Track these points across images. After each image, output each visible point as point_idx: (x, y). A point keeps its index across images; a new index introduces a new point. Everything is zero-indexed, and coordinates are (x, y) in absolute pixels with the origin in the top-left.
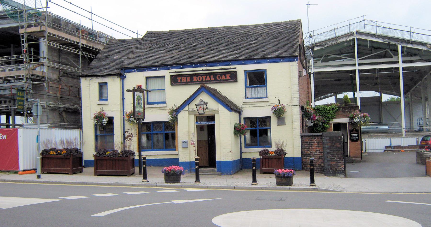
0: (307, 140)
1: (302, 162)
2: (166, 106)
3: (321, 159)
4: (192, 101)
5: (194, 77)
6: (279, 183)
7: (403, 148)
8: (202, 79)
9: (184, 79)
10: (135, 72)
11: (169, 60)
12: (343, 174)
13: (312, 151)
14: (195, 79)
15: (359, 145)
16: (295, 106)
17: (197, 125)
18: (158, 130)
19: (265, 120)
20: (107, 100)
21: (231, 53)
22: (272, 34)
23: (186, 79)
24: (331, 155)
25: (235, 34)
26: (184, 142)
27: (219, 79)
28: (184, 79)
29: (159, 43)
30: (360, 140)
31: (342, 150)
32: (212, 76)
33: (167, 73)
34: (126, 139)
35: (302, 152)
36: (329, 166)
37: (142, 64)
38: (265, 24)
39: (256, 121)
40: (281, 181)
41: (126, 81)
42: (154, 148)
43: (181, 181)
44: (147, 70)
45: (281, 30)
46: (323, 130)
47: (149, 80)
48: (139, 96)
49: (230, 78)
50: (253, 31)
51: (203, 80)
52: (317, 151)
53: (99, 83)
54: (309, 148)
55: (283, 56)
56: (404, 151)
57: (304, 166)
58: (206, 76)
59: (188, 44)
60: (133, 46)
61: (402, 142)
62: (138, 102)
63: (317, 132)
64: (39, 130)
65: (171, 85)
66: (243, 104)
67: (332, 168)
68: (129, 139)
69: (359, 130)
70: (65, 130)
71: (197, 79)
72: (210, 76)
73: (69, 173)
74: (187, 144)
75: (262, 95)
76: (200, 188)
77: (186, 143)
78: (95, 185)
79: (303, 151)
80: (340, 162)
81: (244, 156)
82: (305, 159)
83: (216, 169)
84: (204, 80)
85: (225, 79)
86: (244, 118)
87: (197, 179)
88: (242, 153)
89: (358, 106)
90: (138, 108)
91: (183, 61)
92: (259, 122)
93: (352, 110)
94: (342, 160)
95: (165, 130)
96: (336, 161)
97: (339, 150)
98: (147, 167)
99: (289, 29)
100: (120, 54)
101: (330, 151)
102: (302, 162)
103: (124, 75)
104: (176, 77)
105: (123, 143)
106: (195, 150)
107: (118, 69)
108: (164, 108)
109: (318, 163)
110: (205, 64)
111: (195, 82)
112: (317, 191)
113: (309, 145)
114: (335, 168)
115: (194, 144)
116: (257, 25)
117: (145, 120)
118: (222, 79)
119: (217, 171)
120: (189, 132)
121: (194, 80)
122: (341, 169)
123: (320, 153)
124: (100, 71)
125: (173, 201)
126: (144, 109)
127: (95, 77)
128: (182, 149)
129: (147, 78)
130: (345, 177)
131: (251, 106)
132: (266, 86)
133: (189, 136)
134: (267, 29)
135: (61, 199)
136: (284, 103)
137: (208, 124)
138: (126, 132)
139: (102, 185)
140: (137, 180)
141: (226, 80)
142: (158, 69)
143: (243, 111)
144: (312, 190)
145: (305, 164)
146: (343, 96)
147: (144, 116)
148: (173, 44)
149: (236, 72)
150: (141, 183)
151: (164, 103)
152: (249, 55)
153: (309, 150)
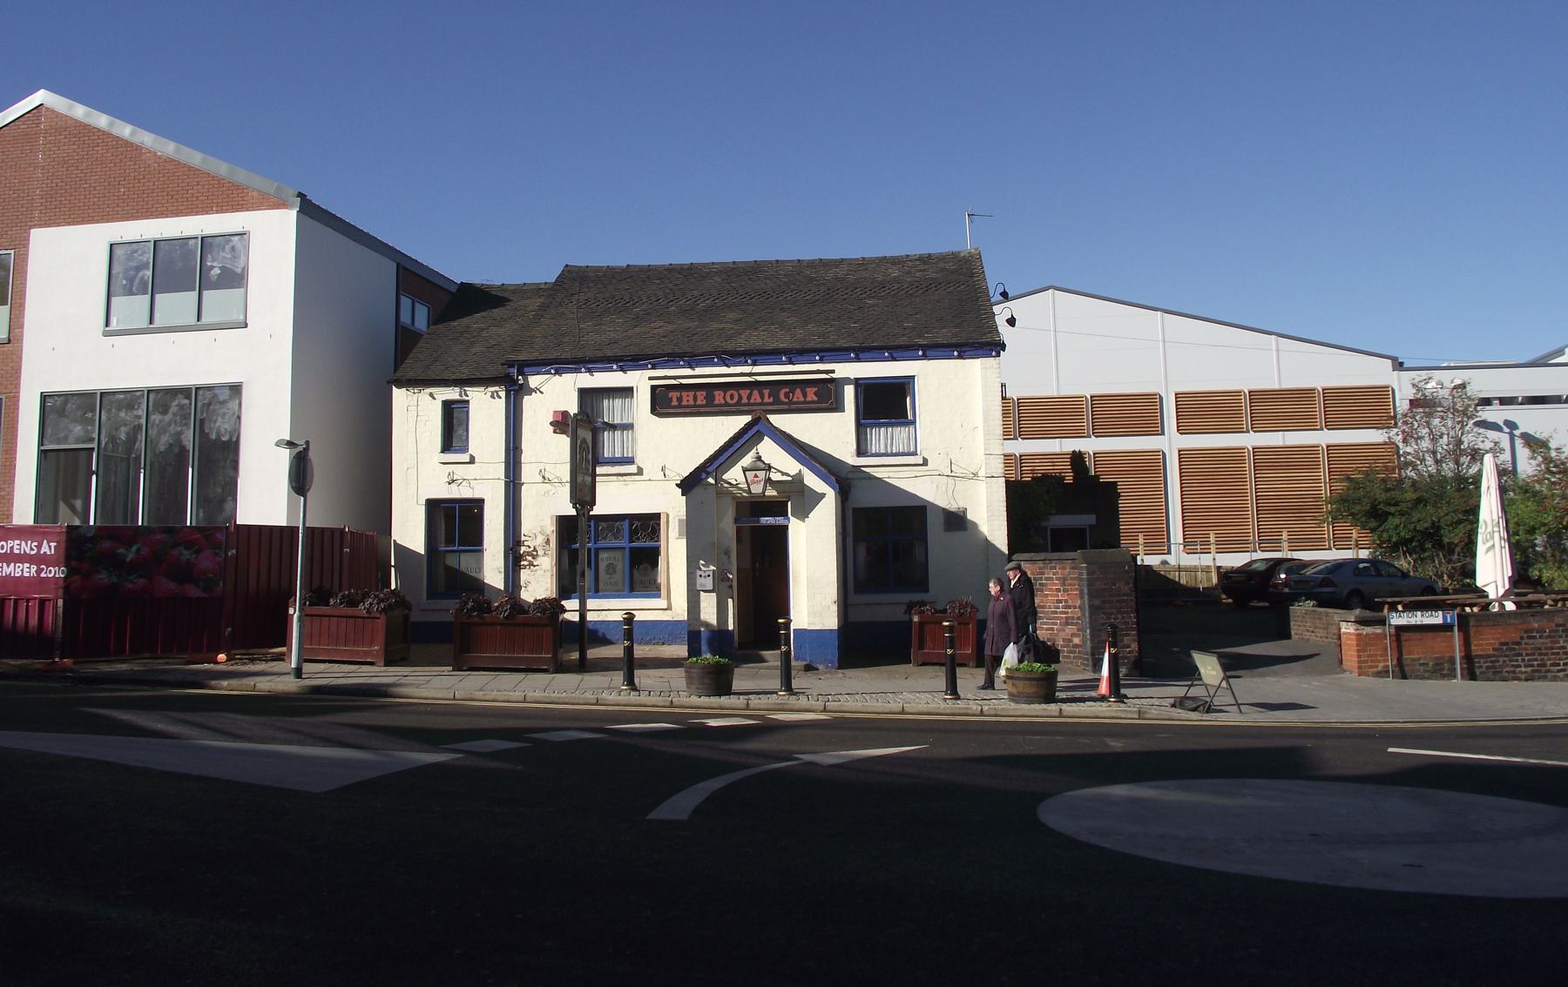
3: (1072, 624)
6: (1014, 696)
8: (740, 398)
14: (719, 397)
16: (993, 477)
24: (1104, 613)
27: (787, 400)
28: (688, 398)
32: (766, 392)
48: (584, 441)
49: (816, 399)
51: (743, 402)
52: (1060, 601)
71: (725, 400)
80: (1128, 635)
84: (745, 401)
89: (798, 479)
95: (631, 541)
117: (596, 511)
118: (795, 399)
121: (717, 402)
123: (1066, 607)
134: (895, 272)
141: (805, 402)
142: (817, 358)
151: (630, 461)
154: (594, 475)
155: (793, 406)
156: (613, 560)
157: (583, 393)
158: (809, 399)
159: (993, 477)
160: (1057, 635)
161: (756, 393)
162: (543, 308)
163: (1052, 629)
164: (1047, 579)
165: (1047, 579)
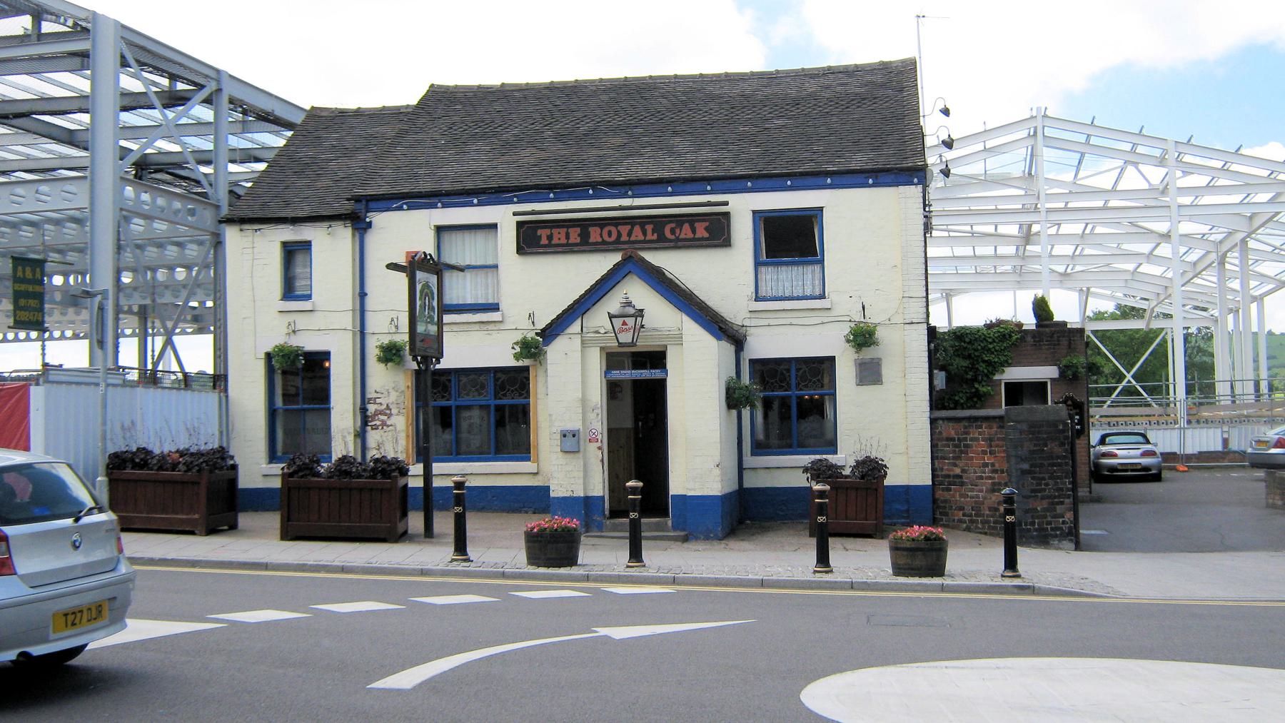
0: (953, 432)
1: (935, 501)
2: (501, 320)
4: (594, 305)
5: (591, 229)
7: (1182, 458)
8: (619, 235)
9: (559, 236)
10: (400, 208)
11: (510, 174)
12: (1071, 540)
13: (967, 465)
15: (1083, 450)
16: (912, 323)
17: (607, 381)
18: (474, 397)
19: (820, 369)
20: (309, 297)
21: (706, 154)
22: (831, 101)
23: (568, 237)
24: (1033, 478)
25: (712, 97)
26: (567, 434)
27: (673, 237)
28: (559, 236)
29: (473, 122)
30: (1086, 433)
31: (1067, 464)
32: (649, 228)
33: (505, 216)
34: (370, 424)
35: (933, 470)
36: (1028, 515)
37: (426, 186)
38: (803, 70)
39: (788, 371)
40: (909, 561)
41: (372, 238)
42: (458, 453)
43: (579, 562)
44: (439, 205)
45: (858, 90)
46: (974, 402)
47: (446, 237)
48: (426, 286)
49: (706, 235)
50: (768, 91)
51: (622, 239)
52: (986, 465)
53: (285, 245)
54: (959, 458)
55: (874, 167)
56: (1186, 469)
57: (941, 513)
58: (629, 227)
59: (567, 126)
60: (390, 131)
61: (1182, 442)
62: (425, 303)
63: (955, 408)
64: (106, 391)
65: (518, 252)
66: (748, 315)
67: (1036, 521)
68: (378, 423)
69: (1083, 403)
70: (152, 389)
71: (601, 237)
72: (644, 226)
73: (196, 532)
74: (579, 442)
75: (790, 288)
76: (653, 583)
77: (574, 436)
78: (295, 571)
79: (936, 466)
80: (1062, 503)
81: (752, 481)
82: (943, 490)
83: (670, 523)
84: (624, 238)
85: (690, 235)
86: (750, 360)
87: (636, 555)
88: (744, 472)
90: (423, 321)
91: (558, 179)
92: (798, 372)
93: (1061, 343)
94: (1069, 497)
96: (1049, 497)
97: (1059, 465)
98: (468, 515)
99: (882, 85)
100: (348, 153)
101: (1031, 466)
102: (935, 501)
103: (368, 220)
104: (535, 229)
105: (361, 435)
106: (602, 461)
107: (348, 200)
108: (493, 324)
109: (988, 503)
110: (627, 187)
111: (596, 244)
112: (1030, 594)
113: (956, 446)
114: (1047, 521)
115: (599, 441)
116: (778, 72)
117: (445, 364)
118: (681, 237)
119: (675, 528)
120: (584, 401)
121: (591, 240)
122: (1064, 522)
123: (995, 471)
124: (287, 204)
125: (603, 631)
126: (440, 329)
127: (270, 223)
128: (561, 454)
129: (440, 230)
130: (1076, 549)
131: (772, 322)
132: (822, 262)
133: (584, 414)
134: (811, 87)
135: (217, 621)
136: (874, 317)
137: (634, 377)
138: (370, 399)
139: (319, 571)
140: (438, 555)
142: (475, 201)
143: (747, 337)
144: (1016, 590)
145: (945, 507)
146: (1033, 299)
147: (441, 351)
148: (516, 125)
149: (727, 215)
150: (451, 567)
151: (494, 307)
152: (768, 163)
153: (957, 462)
154: (440, 324)
155: (680, 244)
156: (474, 421)
157: (440, 230)
158: (698, 235)
159: (912, 323)
160: (983, 503)
161: (637, 229)
162: (401, 134)
163: (978, 497)
164: (972, 440)
165: (972, 440)
